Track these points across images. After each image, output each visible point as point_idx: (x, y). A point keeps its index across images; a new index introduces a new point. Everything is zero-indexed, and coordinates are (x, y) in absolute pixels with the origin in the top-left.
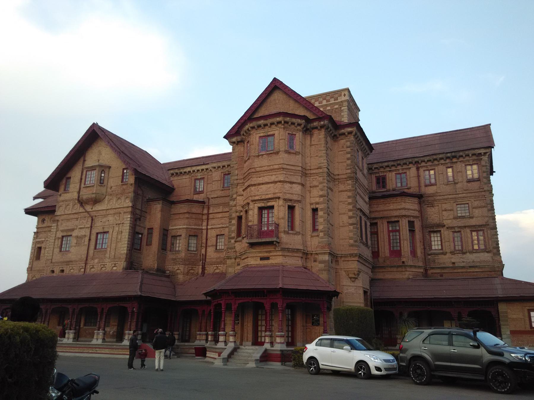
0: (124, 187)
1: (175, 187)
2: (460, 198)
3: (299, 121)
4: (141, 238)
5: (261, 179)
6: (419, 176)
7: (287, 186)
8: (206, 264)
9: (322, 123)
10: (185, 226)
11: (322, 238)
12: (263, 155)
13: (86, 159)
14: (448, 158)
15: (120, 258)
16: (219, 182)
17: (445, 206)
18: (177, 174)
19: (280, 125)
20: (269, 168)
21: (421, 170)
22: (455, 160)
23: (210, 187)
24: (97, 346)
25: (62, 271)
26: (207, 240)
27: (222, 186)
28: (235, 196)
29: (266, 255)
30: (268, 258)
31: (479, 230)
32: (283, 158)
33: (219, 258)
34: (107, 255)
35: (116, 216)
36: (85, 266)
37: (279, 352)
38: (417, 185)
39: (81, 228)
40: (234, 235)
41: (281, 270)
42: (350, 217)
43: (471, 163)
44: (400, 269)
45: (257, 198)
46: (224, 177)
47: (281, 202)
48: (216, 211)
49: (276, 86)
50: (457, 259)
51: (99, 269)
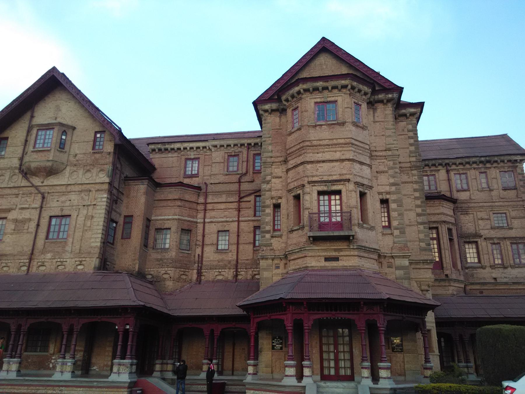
0: (97, 156)
1: (156, 166)
2: (497, 206)
4: (115, 228)
5: (320, 155)
6: (449, 180)
7: (357, 166)
8: (203, 268)
9: (390, 96)
11: (397, 237)
12: (321, 125)
13: (36, 114)
14: (481, 162)
15: (89, 253)
16: (222, 164)
18: (160, 150)
19: (344, 90)
20: (331, 142)
21: (452, 173)
22: (488, 165)
23: (211, 170)
24: (61, 384)
26: (204, 236)
27: (226, 169)
28: (268, 178)
29: (334, 254)
30: (336, 259)
31: (519, 243)
32: (350, 131)
33: (222, 260)
34: (68, 248)
35: (83, 195)
36: (30, 262)
37: (388, 392)
38: (448, 189)
41: (357, 275)
42: (418, 215)
43: (506, 170)
44: (443, 283)
46: (228, 159)
47: (351, 186)
48: (216, 201)
49: (325, 47)
50: (497, 273)
51: (53, 267)
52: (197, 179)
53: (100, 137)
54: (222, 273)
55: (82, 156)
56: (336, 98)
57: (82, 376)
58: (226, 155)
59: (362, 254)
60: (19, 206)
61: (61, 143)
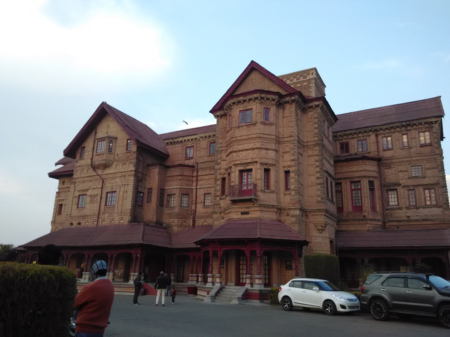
0: (128, 154)
2: (415, 160)
3: (273, 97)
4: (143, 196)
5: (241, 146)
6: (377, 142)
9: (293, 98)
10: (178, 187)
11: (293, 196)
12: (242, 126)
13: (97, 131)
14: (403, 126)
15: (126, 213)
16: (206, 149)
17: (400, 168)
18: (171, 143)
21: (380, 137)
22: (409, 128)
23: (199, 154)
25: (79, 224)
26: (196, 198)
27: (208, 153)
28: (219, 161)
29: (246, 210)
30: (247, 213)
32: (259, 129)
33: (207, 213)
34: (116, 211)
38: (376, 149)
39: (94, 189)
40: (219, 193)
41: (259, 222)
42: (318, 178)
44: (361, 222)
45: (238, 162)
46: (210, 145)
47: (258, 166)
48: (203, 174)
50: (411, 213)
51: (109, 222)
52: (193, 160)
53: (130, 142)
54: (207, 221)
55: (121, 155)
56: (252, 107)
57: (124, 281)
58: (209, 143)
59: (262, 209)
60: (92, 187)
61: (109, 148)
